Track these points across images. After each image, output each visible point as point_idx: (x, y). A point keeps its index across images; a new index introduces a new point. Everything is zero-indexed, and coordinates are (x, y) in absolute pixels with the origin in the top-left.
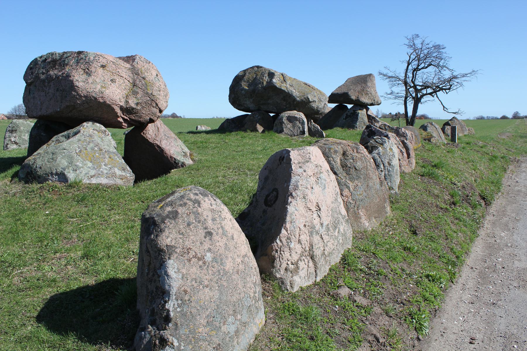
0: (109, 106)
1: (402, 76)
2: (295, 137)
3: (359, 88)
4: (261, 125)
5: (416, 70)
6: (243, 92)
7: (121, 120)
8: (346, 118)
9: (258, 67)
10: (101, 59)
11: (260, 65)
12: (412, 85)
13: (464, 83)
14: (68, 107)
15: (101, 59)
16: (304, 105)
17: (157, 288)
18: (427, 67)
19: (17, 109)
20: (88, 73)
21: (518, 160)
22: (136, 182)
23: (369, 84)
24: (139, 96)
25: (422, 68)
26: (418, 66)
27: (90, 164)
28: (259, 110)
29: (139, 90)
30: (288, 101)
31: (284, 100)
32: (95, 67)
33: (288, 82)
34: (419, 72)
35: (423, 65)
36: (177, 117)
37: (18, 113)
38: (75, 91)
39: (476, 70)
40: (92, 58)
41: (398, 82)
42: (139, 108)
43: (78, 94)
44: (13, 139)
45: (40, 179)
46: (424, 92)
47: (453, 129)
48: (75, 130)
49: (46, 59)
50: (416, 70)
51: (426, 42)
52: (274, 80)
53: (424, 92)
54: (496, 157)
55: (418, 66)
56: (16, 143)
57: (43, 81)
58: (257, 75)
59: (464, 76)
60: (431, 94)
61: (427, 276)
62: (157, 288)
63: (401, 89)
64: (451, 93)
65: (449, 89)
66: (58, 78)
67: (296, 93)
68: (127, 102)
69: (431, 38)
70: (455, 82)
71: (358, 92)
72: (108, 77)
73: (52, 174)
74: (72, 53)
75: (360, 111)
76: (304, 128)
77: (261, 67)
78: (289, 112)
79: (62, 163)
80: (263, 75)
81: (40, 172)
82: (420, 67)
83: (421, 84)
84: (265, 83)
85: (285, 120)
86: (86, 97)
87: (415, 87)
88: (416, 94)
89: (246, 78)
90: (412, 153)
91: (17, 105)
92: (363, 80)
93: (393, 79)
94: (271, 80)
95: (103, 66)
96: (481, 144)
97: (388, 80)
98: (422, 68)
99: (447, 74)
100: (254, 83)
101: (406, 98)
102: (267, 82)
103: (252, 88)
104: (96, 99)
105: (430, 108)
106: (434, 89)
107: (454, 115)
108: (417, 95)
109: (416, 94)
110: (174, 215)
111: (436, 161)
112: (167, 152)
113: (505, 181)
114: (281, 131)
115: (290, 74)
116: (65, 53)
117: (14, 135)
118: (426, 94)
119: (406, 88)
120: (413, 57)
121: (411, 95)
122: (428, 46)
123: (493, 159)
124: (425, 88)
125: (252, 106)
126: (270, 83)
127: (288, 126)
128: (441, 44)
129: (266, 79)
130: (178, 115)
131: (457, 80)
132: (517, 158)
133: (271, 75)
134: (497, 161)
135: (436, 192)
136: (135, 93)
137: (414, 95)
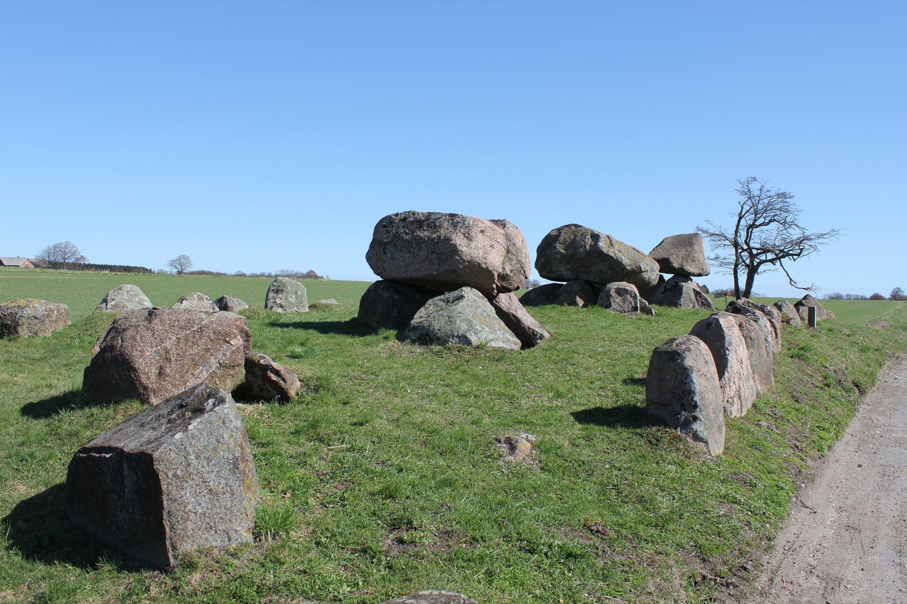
0: (490, 272)
1: (730, 233)
2: (626, 314)
3: (683, 253)
4: (581, 297)
5: (751, 227)
6: (558, 256)
7: (494, 286)
8: (665, 292)
9: (576, 226)
10: (480, 224)
11: (579, 224)
12: (745, 247)
13: (819, 247)
14: (447, 271)
15: (480, 224)
16: (634, 275)
17: (683, 391)
18: (768, 224)
19: (52, 251)
20: (469, 238)
21: (898, 357)
22: (522, 348)
23: (696, 247)
24: (513, 263)
25: (760, 225)
26: (755, 220)
27: (487, 329)
28: (576, 279)
29: (513, 257)
30: (618, 270)
31: (611, 268)
32: (475, 232)
33: (616, 247)
34: (755, 230)
35: (761, 221)
36: (316, 277)
37: (52, 259)
38: (459, 255)
39: (836, 229)
40: (471, 223)
41: (723, 242)
42: (512, 275)
43: (461, 259)
44: (278, 301)
45: (442, 341)
46: (763, 257)
47: (811, 311)
48: (456, 293)
49: (405, 219)
50: (751, 227)
51: (766, 188)
52: (600, 244)
53: (763, 257)
54: (868, 349)
55: (755, 220)
56: (281, 306)
57: (410, 242)
58: (576, 236)
59: (820, 236)
60: (772, 261)
61: (818, 427)
62: (683, 391)
63: (729, 253)
64: (800, 260)
65: (799, 255)
66: (433, 240)
67: (626, 261)
68: (504, 269)
69: (773, 182)
70: (806, 245)
71: (683, 258)
72: (488, 243)
73: (453, 336)
74: (442, 215)
75: (684, 284)
76: (636, 303)
77: (580, 226)
78: (624, 283)
79: (462, 327)
80: (584, 235)
81: (439, 334)
82: (757, 223)
83: (758, 246)
84: (588, 247)
85: (613, 292)
86: (469, 262)
87: (750, 249)
88: (751, 261)
89: (561, 238)
90: (779, 335)
91: (51, 245)
92: (687, 242)
93: (717, 238)
94: (596, 244)
95: (482, 232)
96: (847, 332)
97: (709, 239)
98: (760, 225)
99: (795, 234)
100: (573, 245)
101: (736, 266)
102: (590, 246)
103: (570, 251)
104: (479, 264)
105: (770, 283)
106: (777, 255)
107: (805, 293)
108: (752, 262)
109: (751, 261)
110: (689, 350)
111: (802, 345)
112: (524, 322)
113: (880, 374)
114: (608, 306)
115: (615, 237)
116: (430, 214)
117: (280, 296)
118: (766, 261)
119: (737, 251)
120: (746, 208)
121: (744, 261)
122: (769, 194)
123: (864, 350)
124: (764, 252)
125: (566, 273)
126: (595, 246)
127: (616, 300)
128: (787, 192)
129: (589, 241)
130: (319, 274)
131: (809, 243)
132: (897, 354)
133: (595, 237)
134: (870, 353)
135: (809, 372)
136: (511, 260)
137: (748, 262)
